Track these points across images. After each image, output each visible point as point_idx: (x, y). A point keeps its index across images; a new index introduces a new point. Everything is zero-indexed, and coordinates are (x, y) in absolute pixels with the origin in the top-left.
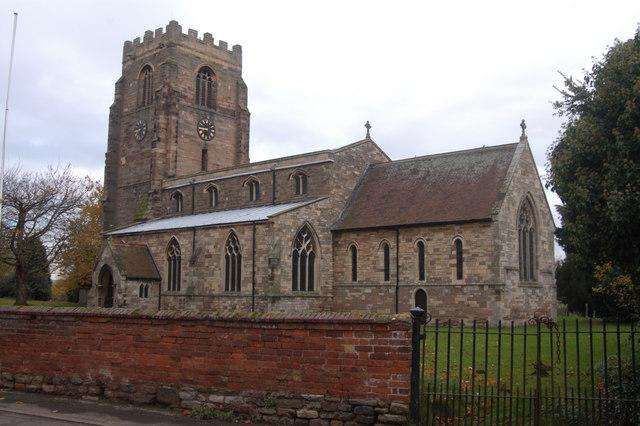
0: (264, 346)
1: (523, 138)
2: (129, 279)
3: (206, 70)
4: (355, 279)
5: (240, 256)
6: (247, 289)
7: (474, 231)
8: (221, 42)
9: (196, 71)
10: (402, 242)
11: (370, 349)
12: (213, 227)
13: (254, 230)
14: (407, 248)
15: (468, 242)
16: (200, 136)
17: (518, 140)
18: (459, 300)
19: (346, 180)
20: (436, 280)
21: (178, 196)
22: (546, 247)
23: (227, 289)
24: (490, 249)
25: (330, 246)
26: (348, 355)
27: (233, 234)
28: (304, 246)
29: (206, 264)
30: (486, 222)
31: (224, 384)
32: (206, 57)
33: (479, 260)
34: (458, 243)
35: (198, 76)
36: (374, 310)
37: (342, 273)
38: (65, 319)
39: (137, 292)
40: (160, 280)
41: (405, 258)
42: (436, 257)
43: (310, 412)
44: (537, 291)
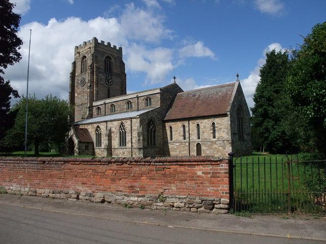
0: (157, 173)
5: (125, 132)
6: (129, 145)
9: (104, 58)
11: (209, 173)
12: (115, 120)
14: (193, 125)
21: (99, 109)
26: (199, 176)
27: (122, 123)
28: (151, 127)
31: (138, 192)
34: (213, 123)
36: (180, 152)
38: (59, 163)
39: (84, 148)
43: (181, 204)
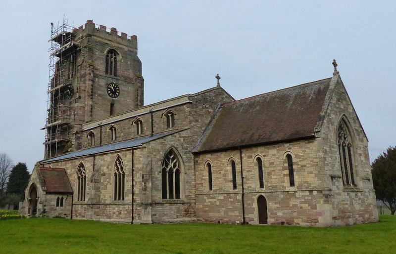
1: (336, 73)
2: (48, 193)
3: (112, 52)
4: (211, 188)
5: (124, 173)
6: (128, 198)
7: (301, 147)
8: (122, 34)
9: (105, 52)
10: (245, 158)
13: (133, 153)
14: (248, 161)
15: (297, 156)
16: (109, 94)
17: (332, 76)
18: (294, 203)
19: (203, 116)
20: (273, 187)
21: (91, 134)
22: (363, 158)
23: (115, 199)
24: (315, 160)
25: (192, 164)
28: (171, 165)
29: (102, 181)
30: (311, 138)
32: (113, 43)
33: (307, 170)
34: (289, 157)
35: (107, 56)
36: (226, 212)
37: (202, 184)
39: (54, 203)
40: (72, 193)
41: (248, 171)
42: (272, 169)
44: (359, 194)
